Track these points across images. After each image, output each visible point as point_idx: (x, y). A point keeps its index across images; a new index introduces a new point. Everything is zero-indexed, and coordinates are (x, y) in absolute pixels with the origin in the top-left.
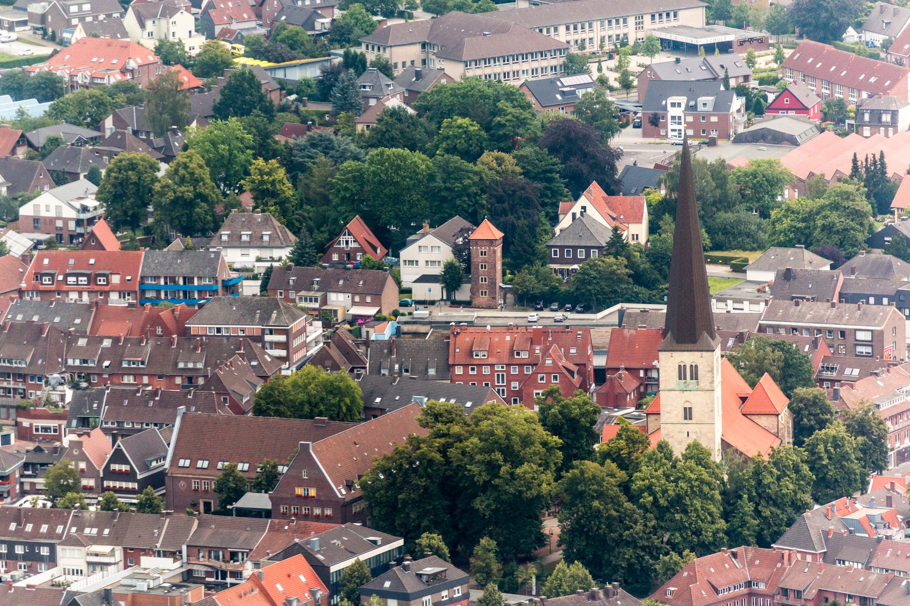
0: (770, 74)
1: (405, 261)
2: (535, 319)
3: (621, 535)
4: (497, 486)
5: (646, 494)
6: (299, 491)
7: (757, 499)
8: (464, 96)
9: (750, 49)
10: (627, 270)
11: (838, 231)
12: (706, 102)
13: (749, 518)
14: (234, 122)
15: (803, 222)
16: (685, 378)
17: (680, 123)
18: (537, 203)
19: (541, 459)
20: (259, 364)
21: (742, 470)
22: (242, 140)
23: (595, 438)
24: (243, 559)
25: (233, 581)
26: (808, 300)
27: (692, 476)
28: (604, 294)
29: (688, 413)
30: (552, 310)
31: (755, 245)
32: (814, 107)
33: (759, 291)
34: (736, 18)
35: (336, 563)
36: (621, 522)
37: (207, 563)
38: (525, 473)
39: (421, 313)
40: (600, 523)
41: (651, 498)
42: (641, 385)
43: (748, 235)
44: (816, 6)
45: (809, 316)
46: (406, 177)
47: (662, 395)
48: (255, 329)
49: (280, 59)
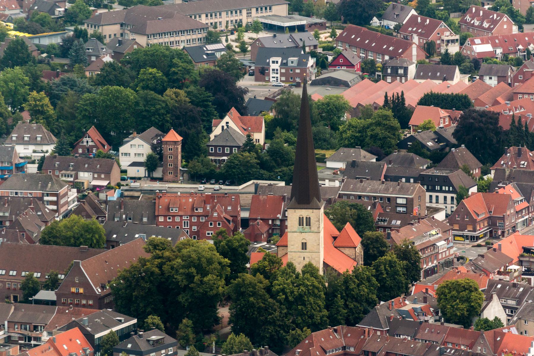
0: (329, 44)
1: (122, 154)
2: (202, 189)
3: (266, 318)
4: (192, 288)
5: (281, 294)
6: (73, 290)
7: (346, 298)
8: (152, 55)
9: (316, 30)
11: (380, 138)
12: (293, 60)
13: (341, 309)
14: (17, 69)
15: (359, 133)
16: (303, 225)
17: (277, 73)
18: (200, 120)
19: (218, 272)
20: (42, 214)
21: (337, 280)
22: (22, 80)
23: (247, 260)
24: (41, 330)
26: (368, 179)
27: (309, 283)
28: (243, 174)
29: (304, 246)
31: (329, 147)
32: (357, 64)
34: (306, 11)
35: (98, 332)
36: (266, 310)
37: (20, 332)
38: (209, 280)
39: (134, 185)
40: (254, 311)
41: (284, 296)
42: (270, 229)
43: (325, 140)
44: (355, 4)
46: (123, 103)
47: (289, 235)
48: (38, 192)
49: (35, 32)
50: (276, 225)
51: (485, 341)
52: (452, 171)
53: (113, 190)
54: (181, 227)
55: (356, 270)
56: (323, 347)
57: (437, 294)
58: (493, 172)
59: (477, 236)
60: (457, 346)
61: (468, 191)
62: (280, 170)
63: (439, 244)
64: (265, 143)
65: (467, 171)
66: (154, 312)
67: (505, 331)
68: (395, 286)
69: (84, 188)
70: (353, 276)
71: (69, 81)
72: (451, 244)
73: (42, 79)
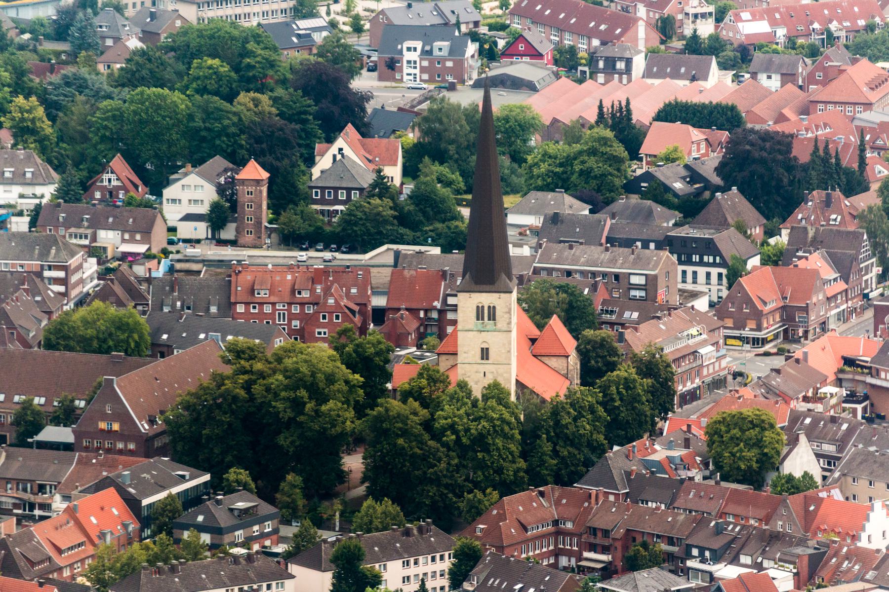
0: (498, 19)
1: (168, 200)
2: (304, 258)
3: (425, 473)
4: (302, 423)
5: (449, 433)
6: (103, 425)
7: (555, 439)
8: (212, 37)
10: (392, 212)
11: (596, 176)
12: (442, 47)
13: (548, 458)
16: (483, 319)
17: (415, 68)
20: (43, 299)
21: (539, 411)
24: (51, 492)
25: (41, 513)
26: (581, 244)
27: (495, 416)
28: (370, 234)
29: (485, 354)
30: (317, 250)
31: (508, 189)
33: (520, 234)
35: (148, 496)
37: (15, 495)
38: (330, 410)
39: (190, 251)
40: (404, 460)
41: (454, 437)
42: (421, 325)
45: (583, 259)
46: (166, 116)
48: (34, 264)
50: (430, 319)
51: (789, 511)
52: (718, 231)
53: (156, 261)
54: (274, 322)
55: (570, 394)
56: (522, 521)
57: (706, 433)
58: (785, 233)
59: (763, 339)
60: (742, 519)
61: (746, 264)
62: (431, 228)
63: (702, 351)
64: (402, 184)
65: (742, 229)
66: (240, 462)
67: (823, 495)
68: (634, 420)
69: (107, 257)
70: (567, 403)
71: (75, 79)
72: (723, 352)
73: (32, 77)
